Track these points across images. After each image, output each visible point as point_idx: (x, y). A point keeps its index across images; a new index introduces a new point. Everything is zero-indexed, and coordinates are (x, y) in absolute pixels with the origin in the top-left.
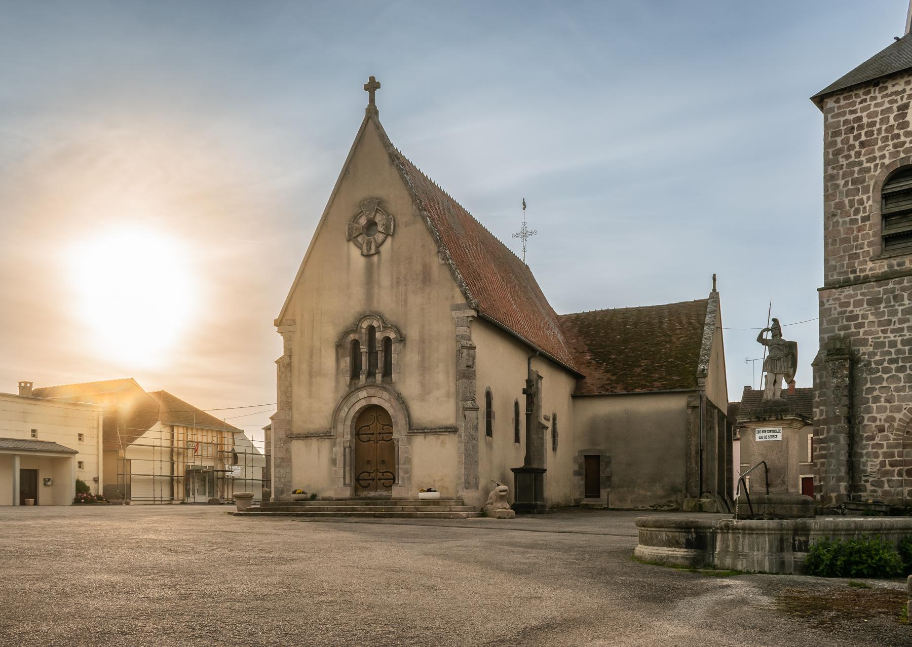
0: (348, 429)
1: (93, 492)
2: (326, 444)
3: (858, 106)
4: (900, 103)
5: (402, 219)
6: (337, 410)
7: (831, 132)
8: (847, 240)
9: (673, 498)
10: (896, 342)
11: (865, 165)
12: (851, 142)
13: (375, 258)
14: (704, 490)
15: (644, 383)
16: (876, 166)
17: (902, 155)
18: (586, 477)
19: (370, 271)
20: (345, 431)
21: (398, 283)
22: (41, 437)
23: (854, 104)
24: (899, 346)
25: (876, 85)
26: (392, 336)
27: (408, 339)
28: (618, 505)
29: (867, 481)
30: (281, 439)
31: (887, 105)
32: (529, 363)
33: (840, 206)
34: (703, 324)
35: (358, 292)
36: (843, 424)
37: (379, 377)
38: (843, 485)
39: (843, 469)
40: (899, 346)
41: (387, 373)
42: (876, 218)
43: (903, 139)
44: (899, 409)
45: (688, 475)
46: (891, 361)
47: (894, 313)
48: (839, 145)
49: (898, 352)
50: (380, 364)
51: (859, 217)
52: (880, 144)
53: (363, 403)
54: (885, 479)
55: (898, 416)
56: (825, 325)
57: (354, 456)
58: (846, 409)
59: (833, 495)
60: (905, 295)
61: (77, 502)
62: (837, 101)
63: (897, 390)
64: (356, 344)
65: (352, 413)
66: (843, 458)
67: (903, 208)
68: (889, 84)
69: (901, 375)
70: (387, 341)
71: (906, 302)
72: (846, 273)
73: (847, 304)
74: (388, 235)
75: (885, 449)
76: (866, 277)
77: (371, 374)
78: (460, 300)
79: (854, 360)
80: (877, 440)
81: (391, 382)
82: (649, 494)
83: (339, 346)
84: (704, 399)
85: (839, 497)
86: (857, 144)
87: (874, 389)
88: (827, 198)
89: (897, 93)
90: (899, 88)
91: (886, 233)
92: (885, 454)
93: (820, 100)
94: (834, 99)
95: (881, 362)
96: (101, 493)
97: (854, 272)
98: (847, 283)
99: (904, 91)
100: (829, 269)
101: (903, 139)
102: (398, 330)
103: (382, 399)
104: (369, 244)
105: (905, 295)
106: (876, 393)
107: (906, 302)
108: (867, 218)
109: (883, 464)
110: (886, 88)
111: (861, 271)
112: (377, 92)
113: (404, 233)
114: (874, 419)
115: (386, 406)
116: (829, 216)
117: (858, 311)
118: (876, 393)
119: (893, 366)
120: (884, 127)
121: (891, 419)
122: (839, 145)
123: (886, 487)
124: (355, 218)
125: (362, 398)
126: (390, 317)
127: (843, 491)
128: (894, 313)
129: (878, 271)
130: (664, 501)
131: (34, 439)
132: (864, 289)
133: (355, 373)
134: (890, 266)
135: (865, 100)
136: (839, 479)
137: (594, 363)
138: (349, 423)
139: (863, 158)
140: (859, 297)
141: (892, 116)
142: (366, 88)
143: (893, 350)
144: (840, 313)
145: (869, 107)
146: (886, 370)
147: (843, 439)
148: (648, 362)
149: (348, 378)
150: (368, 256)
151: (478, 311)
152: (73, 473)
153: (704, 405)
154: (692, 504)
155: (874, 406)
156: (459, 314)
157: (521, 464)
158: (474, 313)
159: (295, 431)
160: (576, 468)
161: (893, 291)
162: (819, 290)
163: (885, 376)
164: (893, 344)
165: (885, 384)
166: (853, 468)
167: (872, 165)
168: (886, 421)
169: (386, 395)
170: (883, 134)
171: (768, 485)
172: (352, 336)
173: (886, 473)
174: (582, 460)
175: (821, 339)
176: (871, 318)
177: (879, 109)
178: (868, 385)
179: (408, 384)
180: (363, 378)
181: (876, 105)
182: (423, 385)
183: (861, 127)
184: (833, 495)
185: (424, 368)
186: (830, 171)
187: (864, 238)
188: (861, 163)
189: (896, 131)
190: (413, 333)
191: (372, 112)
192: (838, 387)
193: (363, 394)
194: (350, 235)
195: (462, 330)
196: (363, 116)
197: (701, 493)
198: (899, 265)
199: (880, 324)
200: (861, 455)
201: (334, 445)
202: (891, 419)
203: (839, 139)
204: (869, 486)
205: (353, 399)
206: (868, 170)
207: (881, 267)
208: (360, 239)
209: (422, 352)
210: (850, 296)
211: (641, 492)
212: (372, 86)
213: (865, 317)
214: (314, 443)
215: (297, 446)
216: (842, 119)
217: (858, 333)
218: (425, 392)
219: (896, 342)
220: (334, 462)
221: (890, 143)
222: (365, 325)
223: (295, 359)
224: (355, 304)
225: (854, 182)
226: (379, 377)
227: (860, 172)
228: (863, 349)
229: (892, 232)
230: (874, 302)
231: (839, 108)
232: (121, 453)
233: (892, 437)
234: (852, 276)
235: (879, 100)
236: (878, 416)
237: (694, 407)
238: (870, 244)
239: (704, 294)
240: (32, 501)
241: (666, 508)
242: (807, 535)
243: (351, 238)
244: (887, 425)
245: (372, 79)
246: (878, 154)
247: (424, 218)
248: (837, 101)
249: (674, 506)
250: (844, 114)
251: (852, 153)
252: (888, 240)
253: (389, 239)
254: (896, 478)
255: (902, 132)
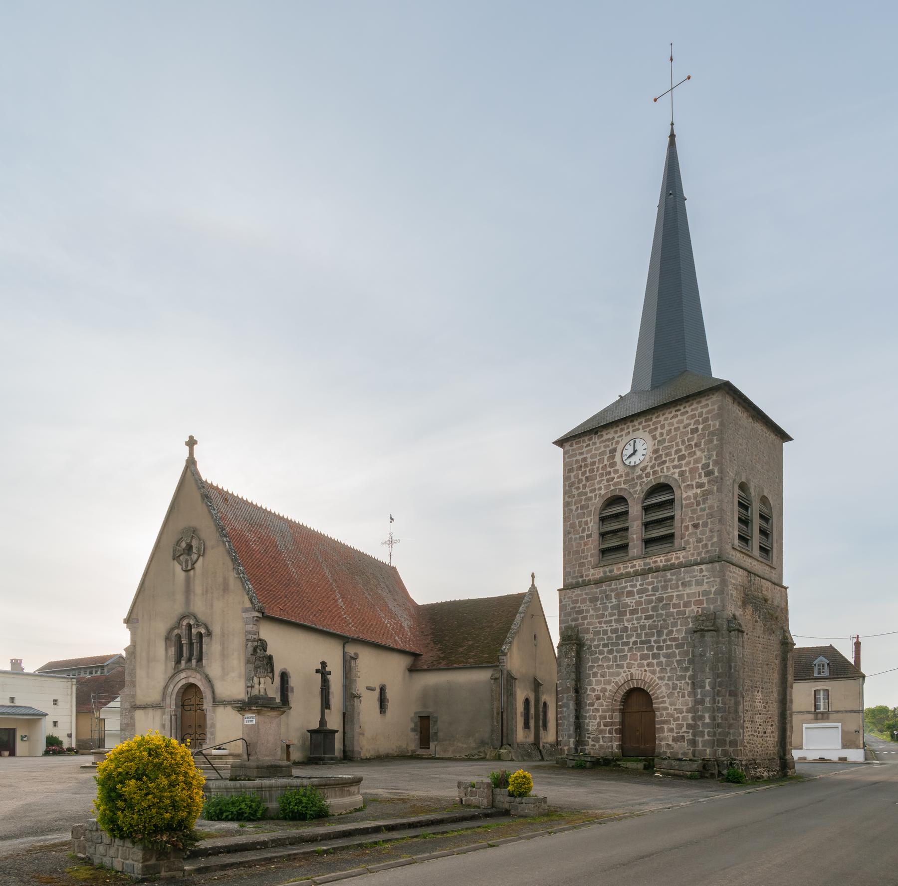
0: (173, 702)
1: (65, 746)
2: (158, 713)
3: (585, 450)
4: (611, 447)
5: (209, 543)
6: (166, 687)
7: (568, 469)
8: (577, 552)
9: (482, 749)
10: (607, 631)
11: (589, 495)
12: (580, 477)
13: (192, 572)
14: (505, 742)
15: (462, 659)
16: (596, 495)
17: (612, 488)
18: (421, 732)
19: (188, 582)
20: (171, 703)
21: (207, 591)
22: (18, 703)
23: (582, 448)
24: (609, 634)
25: (596, 433)
26: (203, 631)
27: (214, 634)
28: (442, 755)
29: (589, 738)
30: (126, 709)
31: (603, 449)
32: (344, 648)
33: (573, 526)
34: (517, 612)
35: (180, 597)
36: (572, 694)
37: (194, 662)
38: (572, 740)
39: (572, 728)
40: (609, 634)
41: (200, 660)
42: (596, 536)
43: (612, 475)
44: (609, 682)
45: (492, 731)
46: (605, 645)
47: (605, 608)
48: (573, 479)
49: (609, 638)
50: (196, 653)
51: (585, 534)
52: (598, 479)
53: (183, 682)
54: (600, 736)
55: (609, 687)
56: (563, 618)
57: (179, 722)
58: (573, 682)
59: (566, 748)
60: (613, 595)
61: (47, 753)
62: (571, 446)
63: (609, 667)
64: (179, 637)
65: (176, 689)
66: (572, 720)
67: (613, 528)
68: (604, 433)
69: (611, 656)
70: (200, 635)
71: (614, 600)
72: (576, 577)
73: (576, 602)
74: (199, 556)
75: (600, 713)
76: (590, 581)
77: (189, 660)
78: (248, 605)
79: (580, 644)
80: (596, 706)
81: (202, 666)
82: (465, 746)
83: (167, 638)
84: (505, 672)
85: (569, 749)
86: (584, 478)
87: (593, 667)
88: (565, 519)
89: (608, 440)
90: (610, 436)
91: (602, 547)
92: (600, 716)
93: (560, 443)
94: (569, 443)
95: (597, 646)
96: (74, 745)
97: (582, 576)
98: (577, 586)
99: (613, 438)
100: (566, 574)
101: (612, 475)
102: (207, 628)
103: (196, 679)
104: (187, 561)
105: (613, 595)
106: (595, 670)
107: (614, 600)
108: (589, 536)
109: (599, 724)
110: (602, 436)
111: (587, 576)
112: (195, 446)
113: (210, 553)
114: (593, 690)
115: (199, 684)
116: (566, 533)
117: (584, 607)
118: (595, 670)
119: (606, 649)
120: (601, 466)
121: (604, 690)
122: (573, 479)
123: (601, 742)
124: (178, 543)
125: (183, 679)
126: (202, 618)
127: (572, 746)
128: (605, 608)
129: (597, 576)
130: (476, 752)
131: (12, 704)
132: (587, 589)
133: (178, 662)
134: (605, 572)
135: (589, 445)
136: (569, 736)
137: (432, 644)
138: (174, 697)
139: (588, 490)
140: (584, 596)
141: (606, 457)
142: (187, 444)
143: (605, 637)
144: (572, 608)
145: (591, 450)
146: (601, 653)
147: (572, 705)
148: (470, 643)
149: (173, 663)
150: (187, 571)
151: (263, 613)
152: (46, 729)
153: (505, 676)
154: (493, 754)
155: (594, 680)
156: (245, 615)
157: (315, 726)
158: (260, 615)
159: (138, 703)
160: (412, 725)
161: (605, 591)
162: (559, 590)
163: (601, 657)
164: (605, 632)
165: (600, 663)
166: (579, 727)
167: (593, 495)
168: (601, 691)
169: (198, 676)
170: (600, 471)
171: (248, 755)
172: (176, 632)
173: (601, 732)
174: (417, 719)
175: (560, 628)
176: (592, 612)
177: (598, 452)
178: (590, 664)
179: (213, 668)
180: (183, 662)
181: (596, 449)
182: (223, 668)
183: (586, 466)
184: (566, 748)
185: (224, 656)
186: (567, 499)
187: (588, 551)
188: (586, 494)
189: (609, 469)
190: (216, 629)
191: (191, 463)
192: (568, 665)
193: (183, 675)
194: (174, 555)
195: (250, 627)
196: (184, 464)
197: (502, 745)
198: (611, 571)
199: (598, 617)
200: (586, 718)
201: (164, 713)
202: (604, 690)
203: (572, 475)
204: (591, 742)
205: (177, 679)
206: (590, 499)
207: (619, 569)
208: (181, 558)
209: (223, 644)
210: (578, 595)
211: (460, 744)
212: (191, 443)
213: (588, 611)
214: (151, 712)
215: (139, 715)
216: (574, 459)
217: (583, 624)
218: (225, 672)
219: (607, 631)
220: (163, 726)
221: (605, 478)
222: (185, 623)
223: (138, 649)
224: (178, 608)
225: (582, 507)
226: (194, 662)
227: (586, 499)
228: (587, 636)
229: (606, 546)
230: (594, 600)
231: (573, 450)
232: (96, 714)
233: (605, 703)
234: (580, 580)
235: (598, 445)
236: (596, 687)
237: (496, 679)
238: (592, 556)
239: (525, 588)
240: (7, 753)
241: (476, 757)
242: (210, 792)
243: (176, 558)
244: (602, 694)
245: (191, 438)
246: (597, 486)
247: (224, 542)
248: (571, 446)
249: (483, 755)
250: (575, 455)
251: (581, 485)
252: (604, 552)
253: (201, 559)
254: (607, 735)
255: (612, 470)
